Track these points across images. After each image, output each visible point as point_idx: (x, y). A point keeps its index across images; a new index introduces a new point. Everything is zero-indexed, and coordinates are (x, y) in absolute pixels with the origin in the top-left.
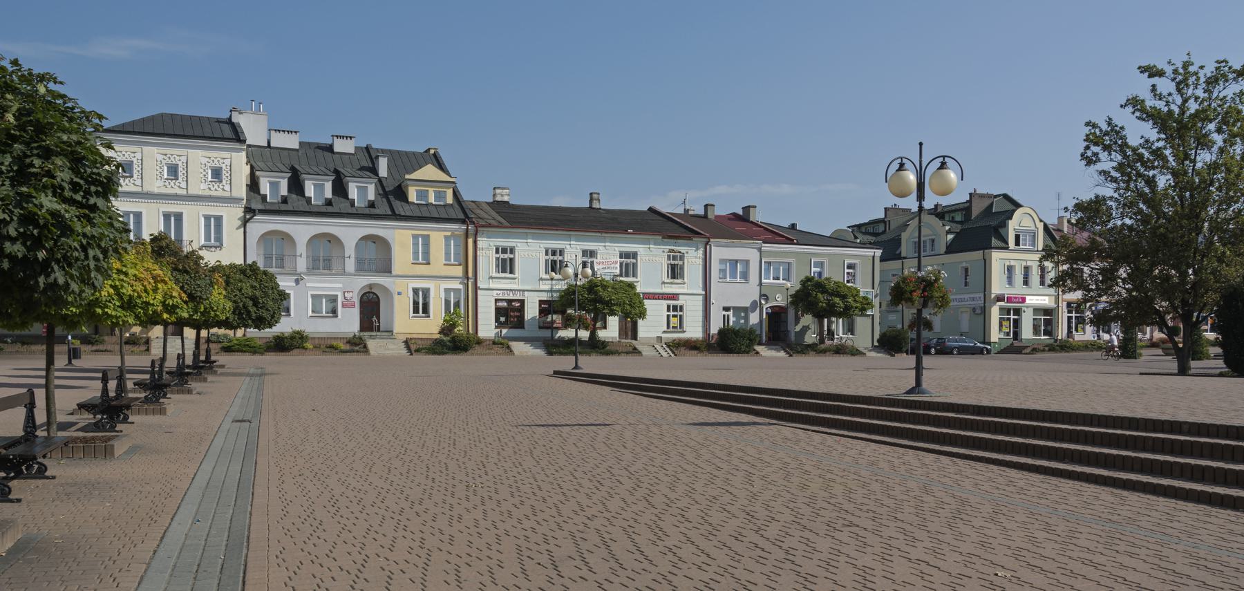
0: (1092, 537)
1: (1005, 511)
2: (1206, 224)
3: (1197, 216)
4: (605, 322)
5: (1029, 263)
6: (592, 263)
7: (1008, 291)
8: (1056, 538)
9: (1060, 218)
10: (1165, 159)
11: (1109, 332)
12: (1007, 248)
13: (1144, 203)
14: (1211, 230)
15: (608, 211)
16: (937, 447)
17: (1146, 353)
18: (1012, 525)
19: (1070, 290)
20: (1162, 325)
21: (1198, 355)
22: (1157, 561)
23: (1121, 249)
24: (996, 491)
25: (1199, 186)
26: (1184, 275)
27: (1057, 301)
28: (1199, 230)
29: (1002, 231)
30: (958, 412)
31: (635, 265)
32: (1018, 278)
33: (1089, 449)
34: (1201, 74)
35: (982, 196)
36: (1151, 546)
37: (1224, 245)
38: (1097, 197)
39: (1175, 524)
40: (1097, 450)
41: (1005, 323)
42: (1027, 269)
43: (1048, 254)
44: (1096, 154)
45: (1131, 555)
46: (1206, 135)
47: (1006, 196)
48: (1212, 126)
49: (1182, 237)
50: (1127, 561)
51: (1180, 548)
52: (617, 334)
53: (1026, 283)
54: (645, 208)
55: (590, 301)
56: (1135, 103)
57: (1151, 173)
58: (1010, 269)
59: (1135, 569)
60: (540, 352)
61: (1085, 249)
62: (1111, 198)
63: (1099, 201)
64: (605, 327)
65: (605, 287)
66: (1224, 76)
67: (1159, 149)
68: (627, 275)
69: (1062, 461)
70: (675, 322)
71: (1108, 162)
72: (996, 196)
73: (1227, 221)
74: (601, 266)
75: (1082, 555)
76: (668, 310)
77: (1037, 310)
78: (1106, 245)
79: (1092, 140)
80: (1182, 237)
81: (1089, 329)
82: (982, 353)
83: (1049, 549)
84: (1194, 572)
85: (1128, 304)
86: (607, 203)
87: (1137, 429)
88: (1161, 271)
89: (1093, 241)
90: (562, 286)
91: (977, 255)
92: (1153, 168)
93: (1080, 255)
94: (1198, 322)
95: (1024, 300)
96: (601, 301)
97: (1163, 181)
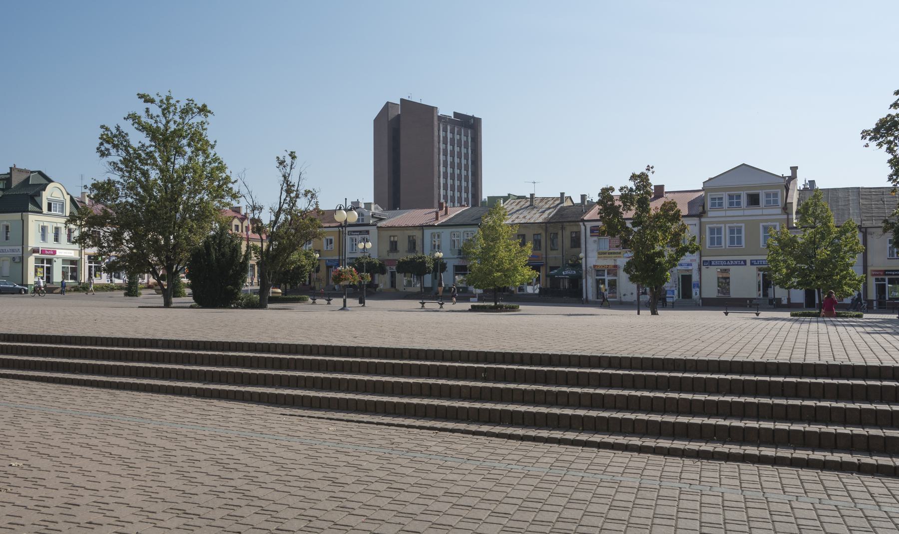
0: (89, 426)
1: (24, 414)
2: (181, 207)
3: (176, 200)
5: (59, 225)
7: (41, 245)
8: (63, 430)
9: (83, 193)
10: (155, 159)
11: (119, 278)
12: (41, 213)
13: (141, 187)
14: (184, 210)
16: (520, 431)
17: (144, 293)
18: (30, 425)
19: (89, 246)
20: (154, 273)
21: (178, 294)
22: (134, 438)
23: (125, 219)
24: (18, 400)
25: (176, 180)
26: (167, 239)
27: (80, 254)
28: (177, 211)
29: (37, 199)
30: (486, 361)
32: (50, 235)
33: (93, 362)
34: (178, 105)
35: (20, 171)
36: (131, 428)
37: (192, 221)
38: (109, 180)
39: (150, 410)
40: (99, 362)
41: (40, 270)
42: (57, 229)
43: (72, 219)
44: (108, 150)
45: (116, 436)
46: (180, 147)
47: (40, 173)
48: (185, 142)
49: (166, 213)
50: (113, 440)
51: (150, 426)
53: (56, 240)
56: (134, 117)
57: (146, 168)
58: (44, 229)
59: (118, 446)
61: (100, 217)
62: (118, 182)
63: (110, 183)
66: (191, 109)
67: (151, 152)
69: (73, 372)
71: (116, 156)
72: (32, 172)
73: (194, 205)
75: (81, 441)
77: (65, 261)
78: (115, 215)
79: (107, 138)
80: (166, 213)
81: (104, 275)
82: (21, 293)
83: (57, 440)
84: (159, 442)
85: (131, 256)
87: (128, 346)
88: (153, 236)
89: (105, 212)
91: (17, 216)
92: (147, 164)
93: (96, 221)
94: (177, 272)
95: (55, 253)
97: (154, 174)
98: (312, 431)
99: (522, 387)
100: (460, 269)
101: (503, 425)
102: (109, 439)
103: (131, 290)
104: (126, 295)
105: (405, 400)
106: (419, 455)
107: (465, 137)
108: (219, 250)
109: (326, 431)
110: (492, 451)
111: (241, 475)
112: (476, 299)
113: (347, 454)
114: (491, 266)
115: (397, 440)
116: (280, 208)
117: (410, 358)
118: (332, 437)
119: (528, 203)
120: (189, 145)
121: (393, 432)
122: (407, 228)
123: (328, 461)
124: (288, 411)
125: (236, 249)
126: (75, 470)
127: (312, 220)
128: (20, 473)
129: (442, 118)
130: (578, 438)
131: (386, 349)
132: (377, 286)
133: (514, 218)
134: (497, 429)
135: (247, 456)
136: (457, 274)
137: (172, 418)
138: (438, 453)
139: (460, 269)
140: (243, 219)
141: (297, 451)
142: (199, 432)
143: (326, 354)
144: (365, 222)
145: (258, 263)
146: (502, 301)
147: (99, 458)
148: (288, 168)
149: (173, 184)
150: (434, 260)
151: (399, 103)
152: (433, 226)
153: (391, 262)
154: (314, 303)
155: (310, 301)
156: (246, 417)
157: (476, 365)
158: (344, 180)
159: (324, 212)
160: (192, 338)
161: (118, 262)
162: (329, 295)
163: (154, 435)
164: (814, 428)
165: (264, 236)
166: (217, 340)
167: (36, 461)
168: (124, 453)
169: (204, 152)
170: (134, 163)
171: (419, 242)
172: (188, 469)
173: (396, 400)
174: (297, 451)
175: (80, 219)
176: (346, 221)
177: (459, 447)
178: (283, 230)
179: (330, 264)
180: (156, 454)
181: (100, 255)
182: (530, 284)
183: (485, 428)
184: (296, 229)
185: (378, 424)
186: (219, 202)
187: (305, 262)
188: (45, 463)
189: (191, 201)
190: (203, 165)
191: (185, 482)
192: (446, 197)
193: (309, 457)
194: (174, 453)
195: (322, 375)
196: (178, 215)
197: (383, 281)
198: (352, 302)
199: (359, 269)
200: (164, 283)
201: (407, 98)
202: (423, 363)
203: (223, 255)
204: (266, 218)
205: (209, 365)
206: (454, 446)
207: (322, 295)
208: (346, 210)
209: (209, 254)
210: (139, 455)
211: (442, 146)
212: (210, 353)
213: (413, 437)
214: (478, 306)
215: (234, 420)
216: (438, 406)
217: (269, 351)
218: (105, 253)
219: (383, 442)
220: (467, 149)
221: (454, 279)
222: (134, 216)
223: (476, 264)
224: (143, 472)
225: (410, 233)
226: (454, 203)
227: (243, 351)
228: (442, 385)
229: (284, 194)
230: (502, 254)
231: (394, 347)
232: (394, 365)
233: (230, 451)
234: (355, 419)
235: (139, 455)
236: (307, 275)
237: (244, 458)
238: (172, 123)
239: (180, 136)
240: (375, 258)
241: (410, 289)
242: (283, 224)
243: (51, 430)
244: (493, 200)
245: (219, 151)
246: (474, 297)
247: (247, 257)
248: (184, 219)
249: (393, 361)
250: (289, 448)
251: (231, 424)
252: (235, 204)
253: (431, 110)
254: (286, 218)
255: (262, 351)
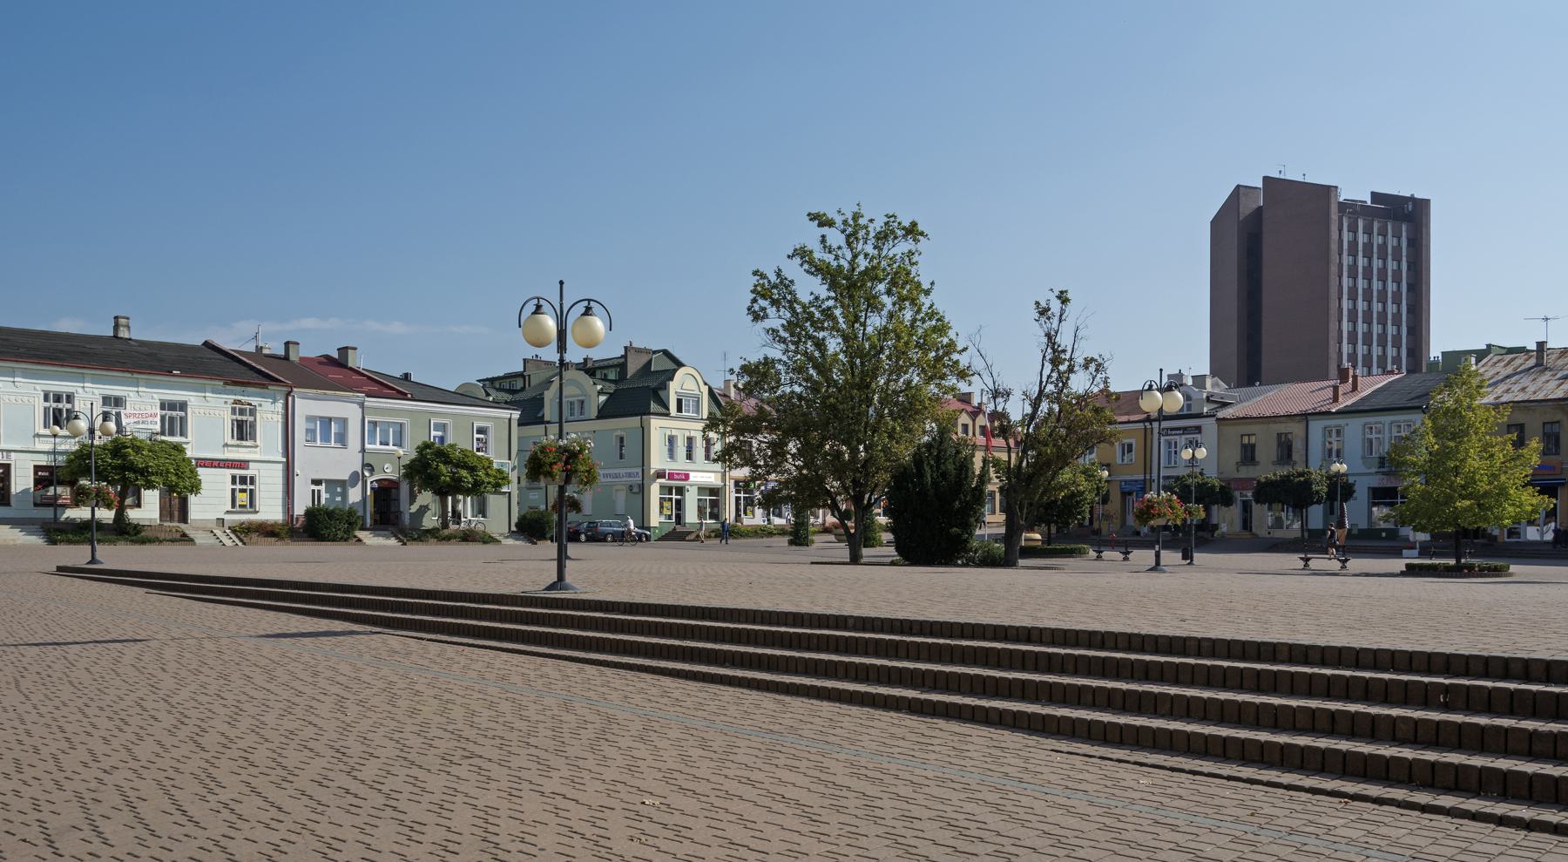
1: (657, 726)
2: (876, 397)
3: (868, 386)
4: (139, 499)
5: (693, 434)
6: (118, 415)
7: (669, 466)
9: (727, 382)
10: (834, 319)
11: (780, 515)
12: (668, 415)
13: (814, 367)
15: (142, 343)
17: (819, 540)
19: (737, 466)
20: (834, 507)
21: (870, 542)
23: (792, 421)
26: (854, 452)
27: (724, 480)
28: (869, 402)
29: (662, 393)
31: (183, 420)
32: (681, 450)
35: (639, 351)
37: (894, 420)
38: (766, 358)
39: (838, 731)
40: (760, 651)
41: (666, 504)
42: (690, 440)
43: (712, 423)
44: (763, 309)
45: (791, 768)
46: (875, 297)
47: (666, 353)
48: (882, 287)
49: (853, 408)
51: (842, 757)
52: (157, 515)
53: (689, 457)
54: (199, 342)
55: (117, 467)
56: (802, 254)
57: (821, 335)
60: (36, 540)
63: (768, 363)
64: (139, 506)
65: (138, 450)
66: (893, 232)
67: (829, 308)
68: (172, 433)
70: (242, 498)
71: (777, 319)
74: (132, 420)
75: (739, 773)
76: (234, 482)
77: (701, 490)
79: (761, 292)
80: (853, 408)
81: (759, 512)
82: (640, 540)
83: (704, 769)
85: (799, 482)
86: (138, 332)
89: (761, 410)
90: (71, 446)
91: (634, 421)
92: (823, 329)
93: (748, 426)
94: (870, 505)
95: (687, 477)
96: (132, 468)
97: (834, 345)
98: (1109, 784)
99: (1529, 725)
100: (1382, 495)
101: (1486, 798)
102: (781, 773)
103: (798, 536)
104: (791, 543)
105: (1283, 739)
106: (1312, 840)
107: (1396, 238)
108: (938, 468)
109: (1132, 784)
110: (1464, 845)
111: (990, 848)
112: (1416, 552)
113: (1174, 828)
114: (1451, 487)
115: (1268, 810)
116: (1041, 392)
117: (1291, 662)
118: (1144, 795)
119: (1532, 362)
120: (889, 292)
121: (1259, 795)
122: (1275, 418)
123: (1140, 838)
124: (1064, 745)
125: (964, 466)
126: (733, 818)
127: (1097, 411)
128: (656, 816)
129: (1352, 209)
130: (1512, 814)
131: (1244, 644)
132: (1216, 527)
133: (1499, 391)
134: (1474, 805)
135: (998, 817)
136: (1375, 504)
137: (874, 746)
138: (1351, 841)
139: (1382, 495)
140: (976, 412)
141: (1084, 817)
142: (917, 771)
143: (1129, 649)
144: (1194, 411)
145: (1001, 489)
146: (1472, 556)
147: (767, 802)
148: (1055, 321)
149: (863, 357)
150: (1329, 478)
151: (1260, 185)
152: (1328, 413)
153: (1243, 483)
154: (1099, 558)
155: (1092, 554)
156: (993, 751)
157: (1426, 680)
158: (1155, 333)
159: (1118, 396)
160: (900, 615)
161: (780, 491)
162: (1127, 543)
163: (848, 771)
164: (1478, 761)
165: (1012, 442)
166: (941, 619)
167: (677, 800)
168: (806, 798)
169: (913, 302)
170: (803, 328)
171: (1298, 445)
172: (903, 832)
173: (1263, 736)
174: (1084, 817)
175: (724, 422)
176: (1161, 410)
177: (1393, 833)
178: (1045, 430)
179: (1128, 488)
180: (852, 802)
181: (754, 479)
182: (1531, 523)
183: (1447, 801)
184: (1068, 428)
185: (1229, 778)
186: (938, 385)
187: (1084, 485)
188: (690, 804)
189: (892, 386)
190: (912, 326)
191: (900, 852)
192: (1353, 358)
193: (1106, 828)
194: (878, 803)
195: (1124, 686)
196: (871, 410)
197: (1227, 519)
198: (1171, 557)
199: (1185, 496)
200: (850, 524)
201: (1277, 175)
202: (1316, 670)
203: (944, 475)
204: (1016, 410)
205: (929, 660)
206: (1383, 830)
207: (1113, 544)
208: (1160, 390)
209: (920, 474)
210: (827, 802)
211: (1346, 260)
212: (930, 640)
213: (1299, 808)
214: (1421, 567)
215: (974, 755)
216: (1348, 752)
217: (1029, 641)
218: (760, 477)
219: (1240, 812)
220: (1399, 262)
221: (1370, 513)
222: (804, 415)
223: (1415, 484)
224: (833, 830)
225: (1282, 428)
226: (1370, 368)
227: (984, 639)
228: (1357, 713)
229: (1048, 367)
230: (1474, 462)
231: (1258, 639)
232: (1259, 672)
233: (969, 807)
234: (1187, 767)
235: (827, 802)
236: (1087, 508)
237: (994, 821)
238: (861, 257)
239: (877, 279)
240: (1212, 476)
241: (1278, 534)
242: (1045, 420)
243: (695, 753)
244: (1454, 359)
245: (938, 300)
246: (1413, 548)
247: (984, 478)
248: (881, 416)
249: (1258, 666)
250: (1070, 811)
251: (968, 763)
252: (963, 387)
253: (1325, 192)
254: (1051, 410)
255: (1018, 640)
